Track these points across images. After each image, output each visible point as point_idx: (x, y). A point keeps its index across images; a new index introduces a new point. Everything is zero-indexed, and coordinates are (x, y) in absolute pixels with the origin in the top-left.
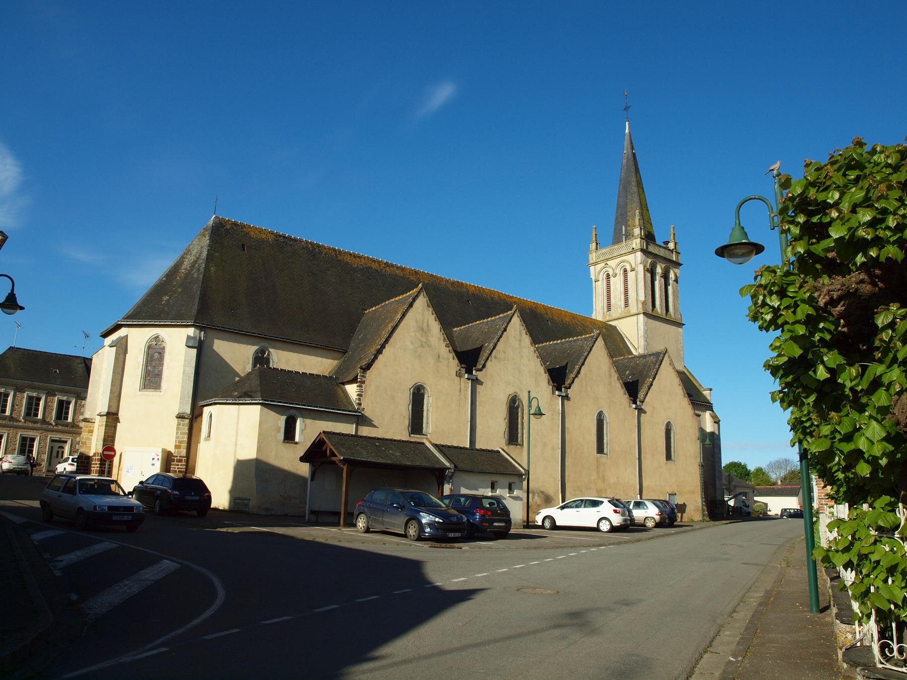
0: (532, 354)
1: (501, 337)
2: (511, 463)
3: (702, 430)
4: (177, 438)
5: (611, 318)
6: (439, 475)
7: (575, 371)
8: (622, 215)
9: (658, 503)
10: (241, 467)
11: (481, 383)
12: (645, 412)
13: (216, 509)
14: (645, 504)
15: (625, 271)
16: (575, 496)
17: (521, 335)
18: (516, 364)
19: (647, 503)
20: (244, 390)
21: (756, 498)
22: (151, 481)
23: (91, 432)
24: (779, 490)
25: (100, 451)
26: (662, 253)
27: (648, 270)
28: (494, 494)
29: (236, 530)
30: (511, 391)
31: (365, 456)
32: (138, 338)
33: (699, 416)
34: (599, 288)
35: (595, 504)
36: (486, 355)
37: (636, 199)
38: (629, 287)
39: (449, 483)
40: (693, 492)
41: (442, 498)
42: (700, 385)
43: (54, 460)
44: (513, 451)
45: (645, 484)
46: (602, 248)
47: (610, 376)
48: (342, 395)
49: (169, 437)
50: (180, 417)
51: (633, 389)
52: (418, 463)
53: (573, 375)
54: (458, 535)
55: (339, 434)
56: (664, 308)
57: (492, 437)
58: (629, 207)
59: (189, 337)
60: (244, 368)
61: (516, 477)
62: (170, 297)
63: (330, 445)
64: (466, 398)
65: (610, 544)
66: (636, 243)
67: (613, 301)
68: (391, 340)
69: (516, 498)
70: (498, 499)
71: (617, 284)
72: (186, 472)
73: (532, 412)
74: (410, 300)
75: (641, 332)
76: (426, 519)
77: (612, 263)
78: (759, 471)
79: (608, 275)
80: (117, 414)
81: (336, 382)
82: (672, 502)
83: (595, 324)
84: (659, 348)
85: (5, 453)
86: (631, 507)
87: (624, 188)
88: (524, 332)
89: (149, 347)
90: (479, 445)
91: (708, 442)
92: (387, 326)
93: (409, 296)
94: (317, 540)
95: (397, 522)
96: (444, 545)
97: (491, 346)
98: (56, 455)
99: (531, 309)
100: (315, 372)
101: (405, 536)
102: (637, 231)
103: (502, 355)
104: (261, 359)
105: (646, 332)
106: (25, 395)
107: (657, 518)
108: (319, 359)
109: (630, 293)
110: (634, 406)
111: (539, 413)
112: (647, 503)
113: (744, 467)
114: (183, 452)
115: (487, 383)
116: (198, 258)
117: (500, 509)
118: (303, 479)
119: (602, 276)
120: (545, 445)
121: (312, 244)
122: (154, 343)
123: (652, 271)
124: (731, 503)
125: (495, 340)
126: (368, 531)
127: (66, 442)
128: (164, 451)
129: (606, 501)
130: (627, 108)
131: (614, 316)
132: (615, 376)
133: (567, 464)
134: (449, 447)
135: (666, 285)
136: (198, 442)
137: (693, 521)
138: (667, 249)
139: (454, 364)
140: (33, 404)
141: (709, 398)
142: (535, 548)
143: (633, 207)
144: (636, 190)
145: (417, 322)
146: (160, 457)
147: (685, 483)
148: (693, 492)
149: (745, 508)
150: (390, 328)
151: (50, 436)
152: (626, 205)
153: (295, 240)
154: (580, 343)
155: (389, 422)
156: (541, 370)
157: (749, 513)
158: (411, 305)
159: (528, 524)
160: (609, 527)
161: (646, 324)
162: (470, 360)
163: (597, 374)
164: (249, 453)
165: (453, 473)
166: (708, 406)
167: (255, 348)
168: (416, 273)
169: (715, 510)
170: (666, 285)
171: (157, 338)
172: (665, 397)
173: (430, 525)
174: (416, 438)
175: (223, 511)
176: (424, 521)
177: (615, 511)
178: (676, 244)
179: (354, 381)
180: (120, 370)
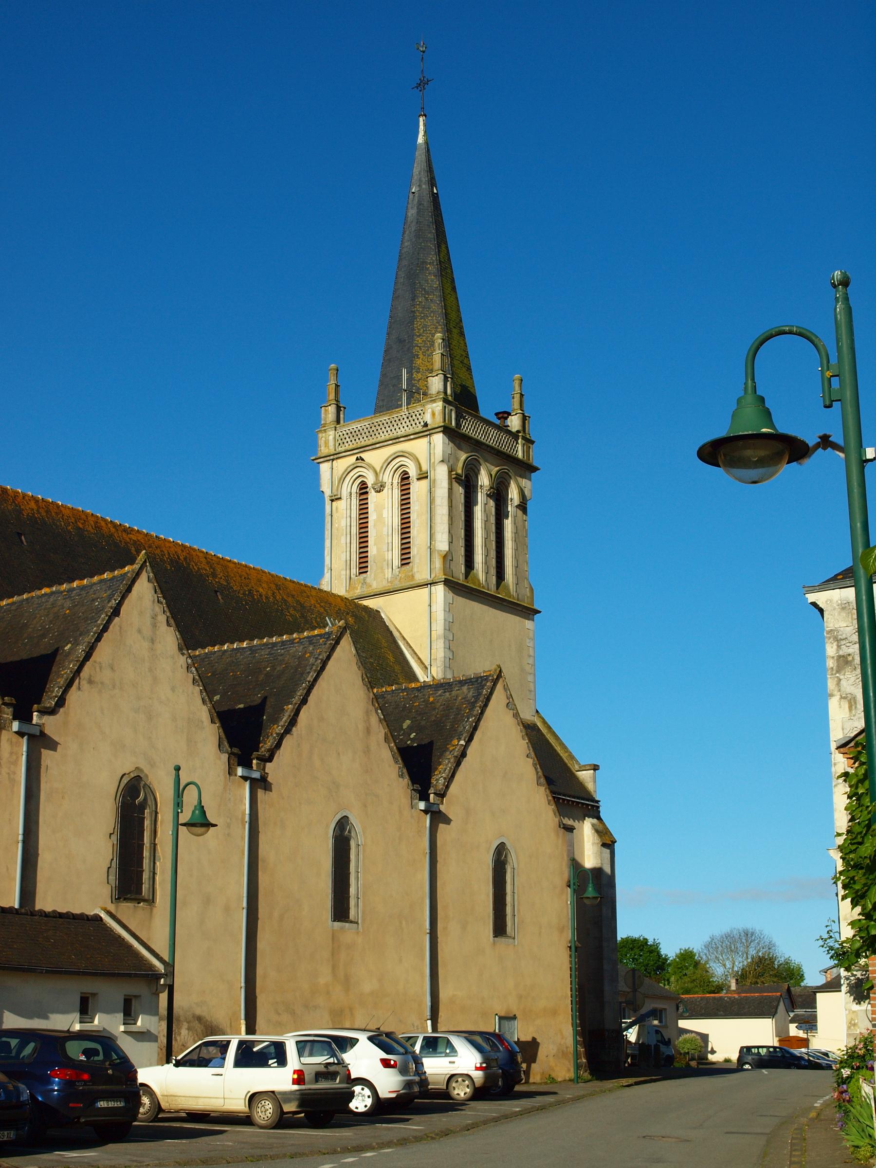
0: (181, 673)
1: (105, 629)
2: (130, 947)
3: (575, 865)
5: (366, 591)
7: (285, 719)
8: (400, 341)
9: (478, 1039)
11: (52, 745)
12: (447, 821)
14: (449, 1044)
15: (405, 478)
17: (154, 626)
19: (455, 1041)
21: (683, 1024)
24: (733, 1002)
26: (492, 438)
27: (458, 479)
28: (87, 1027)
30: (126, 765)
33: (570, 829)
34: (342, 515)
36: (66, 673)
37: (436, 306)
38: (413, 516)
40: (554, 1013)
42: (572, 757)
44: (126, 910)
45: (444, 994)
46: (356, 416)
47: (368, 731)
51: (422, 762)
53: (279, 729)
56: (493, 571)
57: (77, 879)
58: (418, 324)
61: (140, 980)
64: (13, 782)
65: (382, 1145)
66: (433, 412)
67: (372, 550)
69: (143, 1036)
70: (106, 1041)
71: (384, 508)
73: (184, 818)
75: (439, 627)
77: (375, 458)
78: (687, 957)
79: (363, 487)
82: (507, 1036)
83: (327, 600)
84: (481, 666)
86: (417, 1048)
87: (410, 276)
88: (162, 618)
90: (47, 900)
91: (590, 892)
99: (175, 562)
102: (436, 384)
103: (106, 676)
105: (449, 626)
107: (478, 1075)
110: (422, 805)
111: (201, 823)
112: (455, 1041)
115: (68, 745)
117: (113, 1066)
119: (349, 488)
120: (207, 901)
123: (466, 481)
124: (632, 1035)
125: (91, 637)
129: (362, 1037)
130: (422, 84)
132: (379, 731)
133: (262, 945)
135: (500, 515)
137: (553, 1081)
138: (504, 429)
141: (590, 786)
143: (426, 328)
144: (436, 284)
147: (531, 984)
148: (554, 1013)
149: (663, 1048)
154: (298, 649)
156: (203, 713)
157: (670, 1059)
160: (369, 1102)
161: (449, 608)
163: (336, 727)
169: (602, 1055)
170: (500, 515)
172: (493, 779)
177: (386, 1063)
178: (524, 418)
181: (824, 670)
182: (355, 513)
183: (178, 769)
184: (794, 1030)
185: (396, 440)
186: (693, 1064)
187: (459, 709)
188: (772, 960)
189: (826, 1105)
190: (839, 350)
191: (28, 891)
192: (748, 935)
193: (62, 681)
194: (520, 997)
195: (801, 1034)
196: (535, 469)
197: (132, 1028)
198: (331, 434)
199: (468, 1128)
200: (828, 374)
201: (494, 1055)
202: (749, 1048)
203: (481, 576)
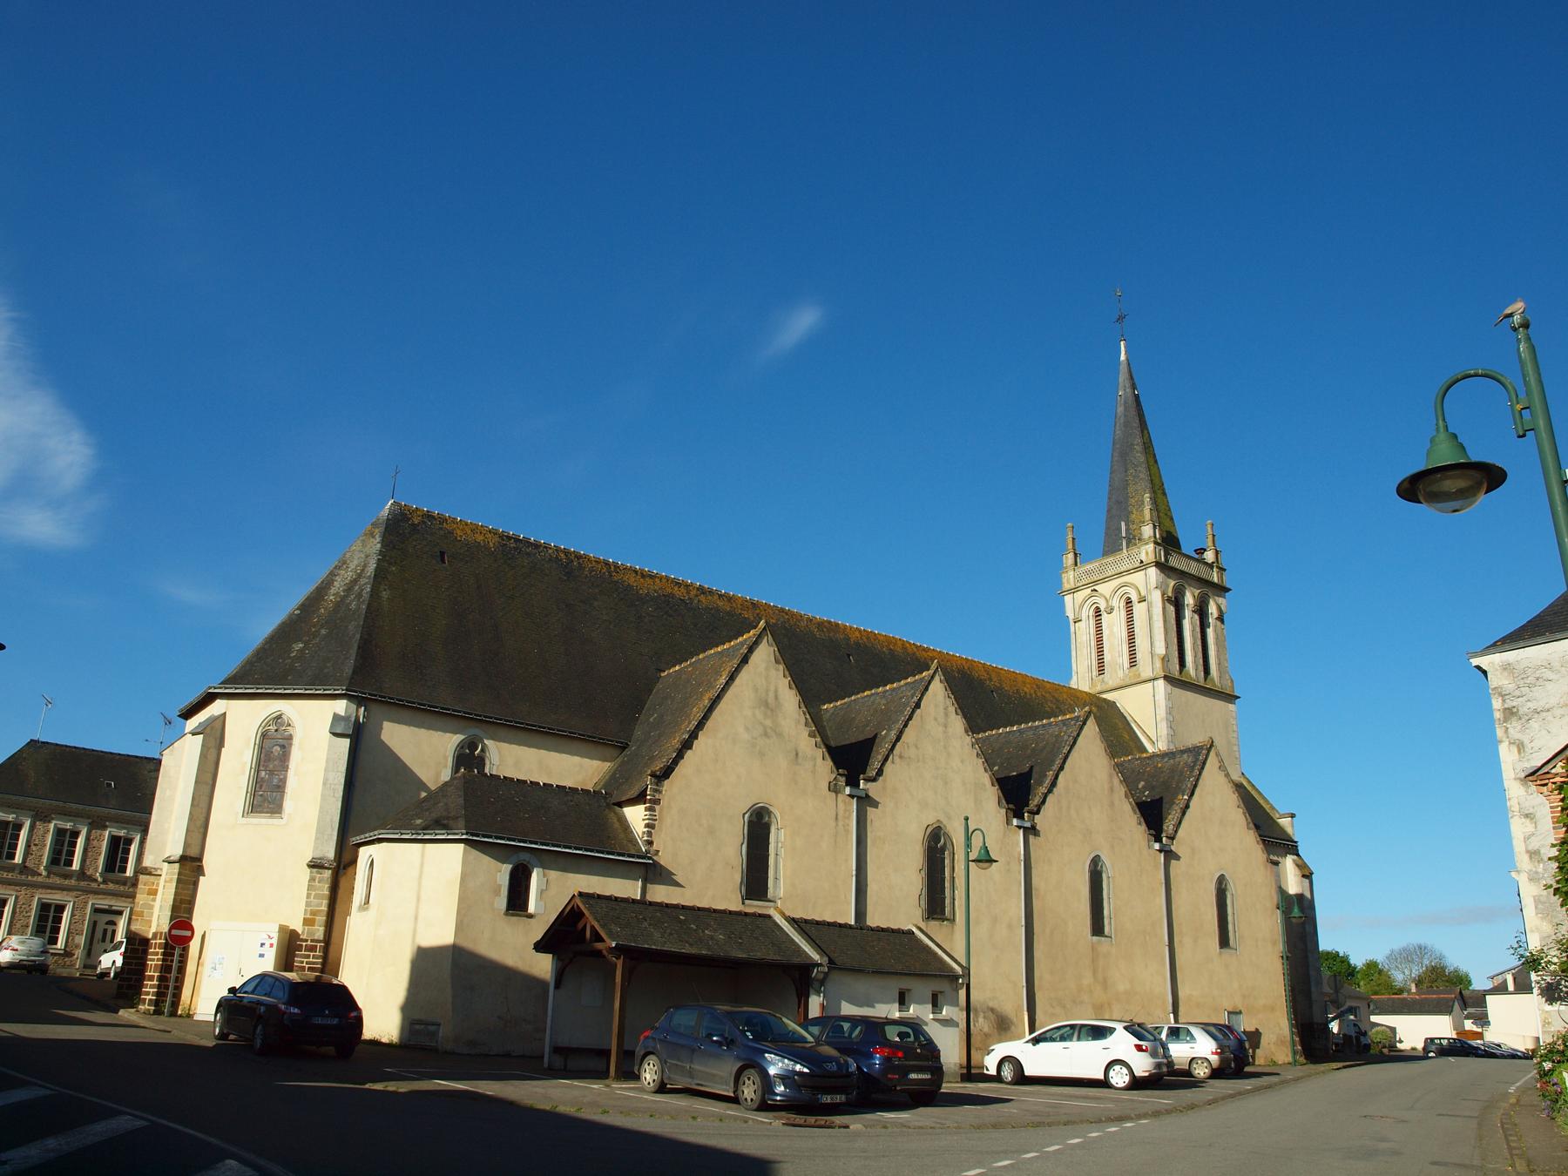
1: (910, 718)
2: (936, 954)
3: (1282, 892)
4: (307, 904)
5: (1105, 688)
6: (801, 978)
7: (1047, 782)
8: (1119, 503)
10: (426, 962)
11: (875, 804)
12: (1177, 858)
13: (375, 1043)
15: (1129, 602)
16: (1054, 1017)
17: (946, 715)
18: (938, 769)
19: (1194, 1031)
20: (434, 815)
21: (1374, 1019)
22: (249, 988)
23: (154, 893)
24: (1414, 1002)
25: (165, 928)
26: (1193, 568)
27: (1169, 600)
28: (904, 1014)
29: (403, 1087)
30: (930, 818)
31: (658, 940)
32: (244, 719)
33: (1276, 863)
34: (1083, 633)
35: (1099, 1033)
37: (1143, 475)
39: (818, 993)
41: (806, 1022)
43: (97, 946)
44: (934, 927)
46: (1088, 561)
47: (1112, 789)
48: (617, 825)
49: (292, 903)
50: (315, 865)
51: (1153, 815)
52: (759, 955)
53: (1043, 790)
54: (840, 1098)
55: (609, 898)
56: (1201, 668)
57: (897, 903)
59: (336, 717)
60: (438, 774)
61: (945, 981)
62: (306, 643)
63: (591, 921)
64: (847, 832)
65: (1139, 1117)
66: (1147, 551)
68: (709, 724)
69: (947, 1023)
70: (915, 1026)
71: (1114, 625)
72: (322, 971)
74: (744, 650)
75: (1162, 712)
76: (776, 1066)
78: (1372, 966)
79: (1098, 610)
80: (200, 859)
81: (609, 799)
83: (1077, 698)
84: (1197, 739)
85: (10, 933)
86: (1163, 1036)
87: (1122, 455)
88: (952, 709)
89: (264, 735)
90: (873, 920)
91: (1296, 912)
92: (701, 699)
93: (742, 644)
94: (562, 1109)
95: (718, 1072)
96: (811, 1120)
97: (893, 735)
98: (100, 937)
99: (962, 672)
100: (568, 783)
101: (735, 1100)
102: (1147, 531)
103: (912, 752)
104: (468, 758)
105: (1170, 711)
106: (52, 826)
107: (1214, 1059)
108: (576, 759)
109: (1138, 641)
110: (1157, 846)
111: (986, 859)
112: (1194, 1031)
113: (1345, 960)
114: (319, 932)
116: (359, 576)
117: (921, 1046)
118: (541, 983)
119: (1087, 612)
121: (566, 552)
122: (273, 728)
123: (1176, 602)
124: (1334, 1027)
125: (900, 725)
126: (662, 1089)
127: (120, 913)
128: (282, 929)
129: (1119, 1027)
130: (1121, 318)
131: (1112, 683)
132: (1121, 790)
133: (1037, 954)
134: (818, 923)
135: (1204, 626)
136: (348, 913)
137: (1275, 1063)
138: (1202, 561)
139: (824, 769)
140: (65, 843)
141: (1289, 830)
142: (994, 1126)
143: (1137, 486)
145: (756, 690)
146: (275, 941)
148: (1273, 1009)
150: (707, 702)
151: (93, 901)
152: (1126, 485)
153: (537, 545)
155: (705, 878)
156: (986, 779)
157: (1367, 1047)
158: (745, 660)
159: (971, 1073)
160: (1127, 1079)
161: (1169, 697)
162: (854, 761)
163: (1087, 786)
164: (441, 933)
165: (826, 974)
166: (1290, 847)
167: (459, 738)
168: (754, 605)
169: (1314, 1044)
170: (1204, 626)
171: (278, 718)
172: (1212, 829)
173: (786, 1078)
174: (754, 907)
175: (389, 1045)
176: (772, 1071)
177: (1139, 1048)
178: (1217, 552)
179: (639, 799)
180: (209, 777)
181: (1492, 721)
182: (1093, 630)
183: (967, 819)
184: (1469, 1025)
185: (1120, 574)
186: (1385, 1051)
187: (1182, 773)
188: (1443, 968)
189: (1523, 1091)
190: (1526, 384)
191: (861, 913)
192: (1422, 950)
193: (880, 757)
194: (1244, 997)
195: (1475, 1028)
196: (1228, 590)
197: (939, 1016)
198: (1071, 573)
199: (1210, 1103)
200: (1519, 407)
201: (1226, 1043)
202: (1432, 1040)
203: (1192, 673)
